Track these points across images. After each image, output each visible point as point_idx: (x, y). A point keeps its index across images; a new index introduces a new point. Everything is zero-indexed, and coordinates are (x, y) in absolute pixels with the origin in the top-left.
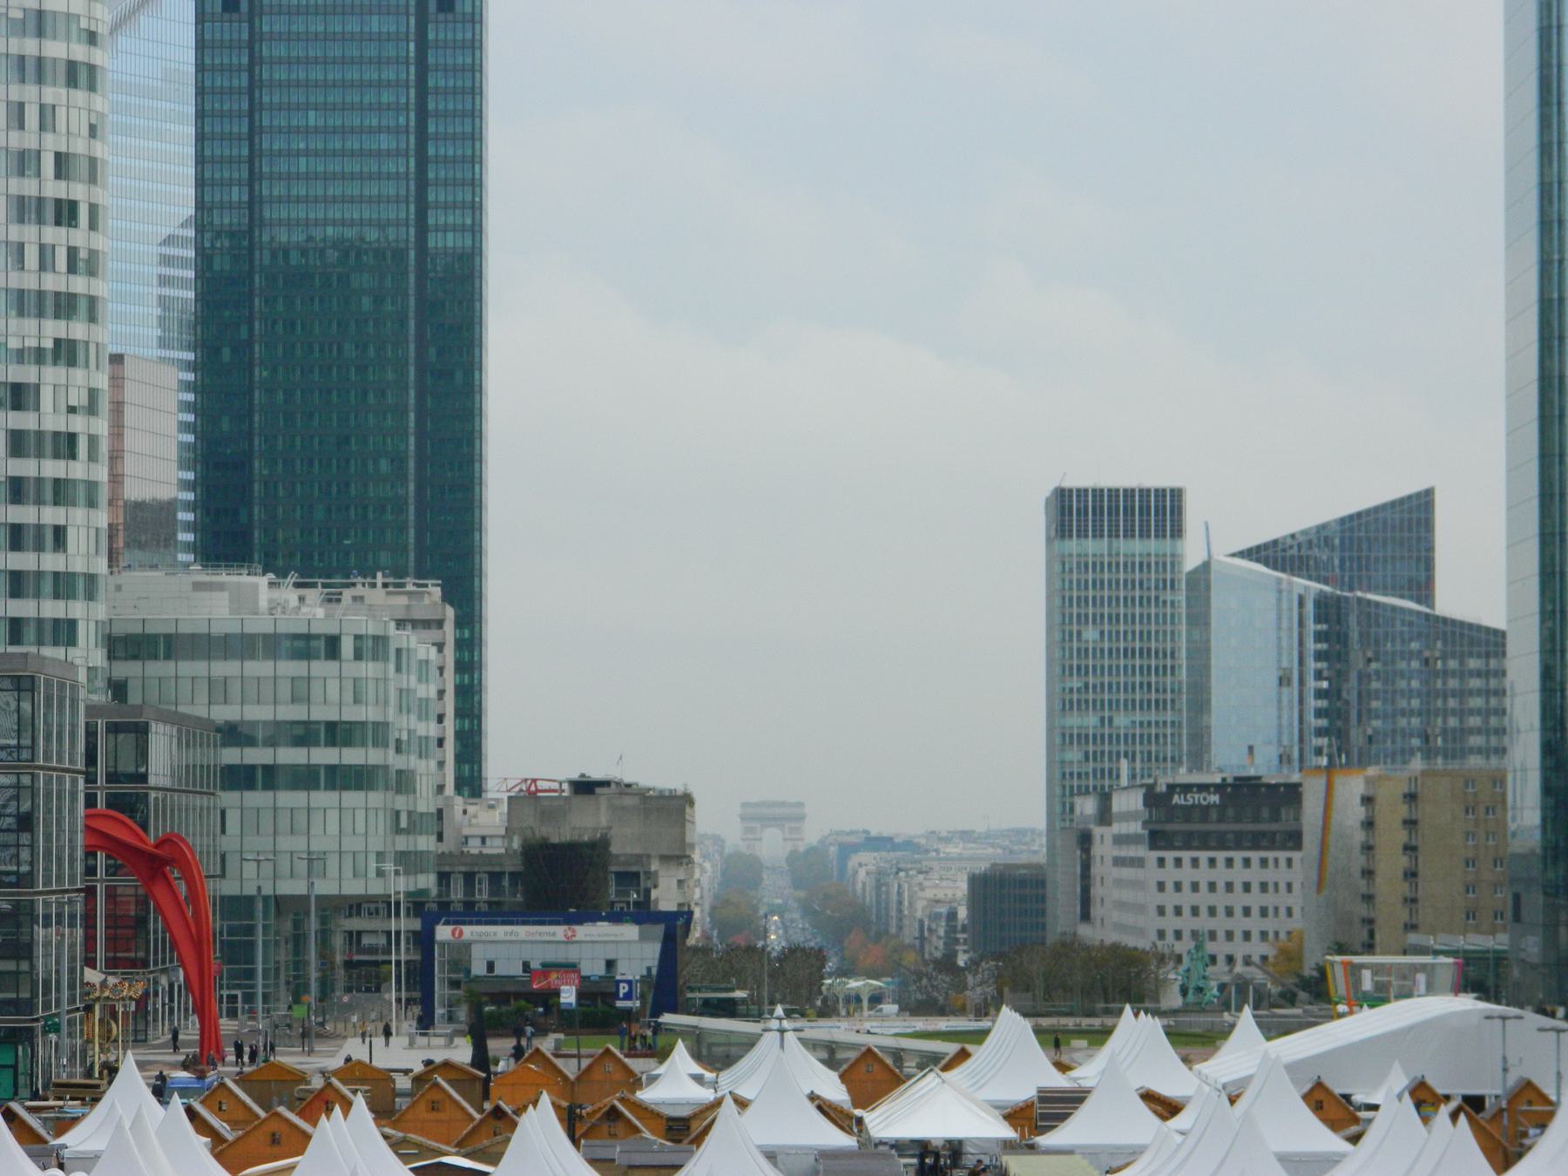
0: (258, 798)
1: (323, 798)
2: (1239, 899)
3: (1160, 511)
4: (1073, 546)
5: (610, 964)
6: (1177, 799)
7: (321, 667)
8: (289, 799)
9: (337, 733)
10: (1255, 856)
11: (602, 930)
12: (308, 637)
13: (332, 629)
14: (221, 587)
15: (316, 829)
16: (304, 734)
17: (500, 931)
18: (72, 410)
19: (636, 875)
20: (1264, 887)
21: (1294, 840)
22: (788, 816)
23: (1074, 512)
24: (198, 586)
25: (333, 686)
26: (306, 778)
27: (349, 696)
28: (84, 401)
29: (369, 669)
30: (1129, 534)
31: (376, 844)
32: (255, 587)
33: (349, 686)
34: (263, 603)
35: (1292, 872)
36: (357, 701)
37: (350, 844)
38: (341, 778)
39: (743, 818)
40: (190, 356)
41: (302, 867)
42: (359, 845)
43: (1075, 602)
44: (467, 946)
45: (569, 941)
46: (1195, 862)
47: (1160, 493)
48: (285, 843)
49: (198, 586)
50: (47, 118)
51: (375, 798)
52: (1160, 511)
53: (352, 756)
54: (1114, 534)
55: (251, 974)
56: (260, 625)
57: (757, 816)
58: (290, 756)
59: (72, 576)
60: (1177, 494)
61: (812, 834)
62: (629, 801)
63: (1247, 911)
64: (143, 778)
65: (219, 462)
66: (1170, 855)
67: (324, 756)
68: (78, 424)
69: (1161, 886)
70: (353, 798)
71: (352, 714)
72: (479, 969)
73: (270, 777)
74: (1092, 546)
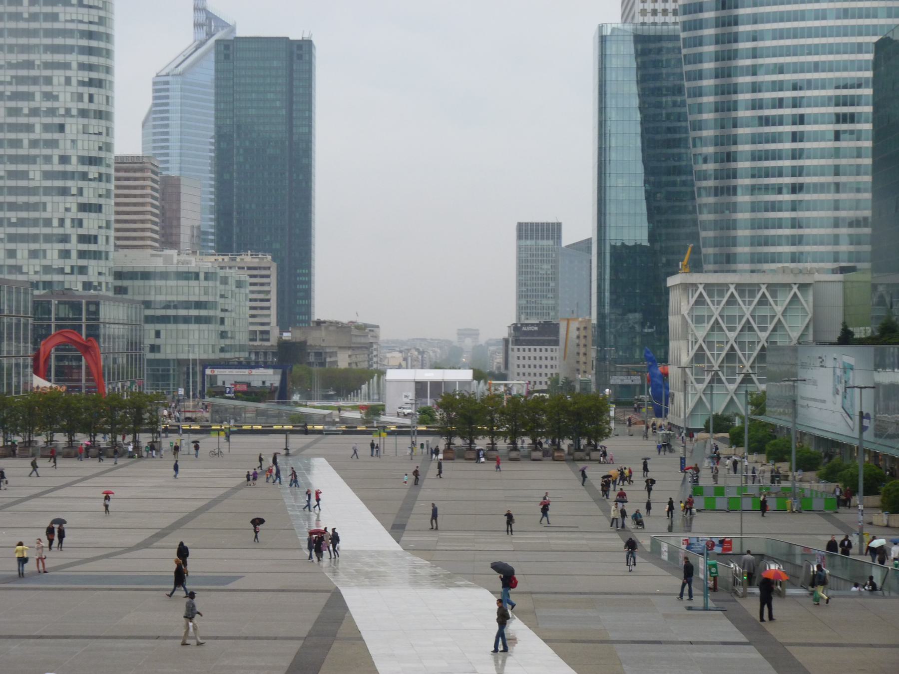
0: (171, 326)
1: (193, 326)
2: (544, 362)
3: (553, 230)
4: (523, 242)
5: (264, 382)
6: (524, 329)
7: (193, 283)
8: (182, 326)
9: (199, 305)
10: (549, 348)
11: (261, 371)
12: (189, 273)
13: (197, 270)
14: (160, 256)
15: (191, 337)
16: (187, 305)
17: (227, 371)
18: (100, 196)
19: (321, 353)
20: (552, 359)
21: (556, 343)
22: (474, 333)
23: (526, 231)
24: (153, 255)
25: (197, 289)
26: (186, 320)
27: (202, 292)
28: (104, 192)
29: (211, 283)
30: (542, 238)
31: (212, 342)
32: (172, 255)
33: (202, 289)
34: (175, 261)
35: (557, 352)
36: (205, 294)
37: (202, 342)
38: (199, 320)
39: (458, 334)
40: (213, 176)
41: (186, 349)
42: (205, 342)
43: (525, 267)
44: (216, 376)
45: (250, 375)
46: (541, 350)
47: (553, 224)
48: (181, 341)
49: (153, 255)
50: (91, 98)
51: (211, 327)
52: (553, 230)
53: (203, 313)
54: (537, 238)
55: (169, 385)
56: (172, 268)
57: (463, 333)
58: (182, 312)
59: (100, 252)
60: (559, 225)
61: (482, 340)
62: (331, 328)
63: (546, 366)
64: (98, 319)
65: (224, 212)
66: (521, 347)
67: (194, 312)
68: (102, 201)
69: (519, 358)
70: (203, 327)
71: (203, 298)
72: (220, 383)
73: (176, 320)
74: (529, 242)
